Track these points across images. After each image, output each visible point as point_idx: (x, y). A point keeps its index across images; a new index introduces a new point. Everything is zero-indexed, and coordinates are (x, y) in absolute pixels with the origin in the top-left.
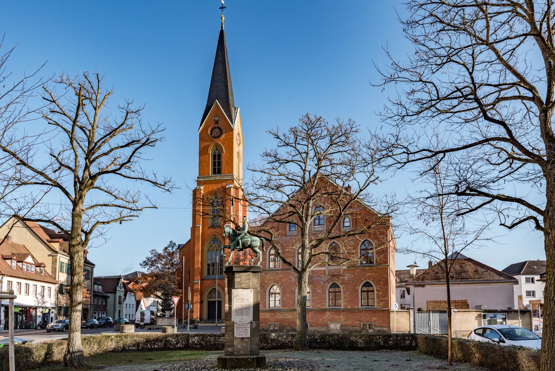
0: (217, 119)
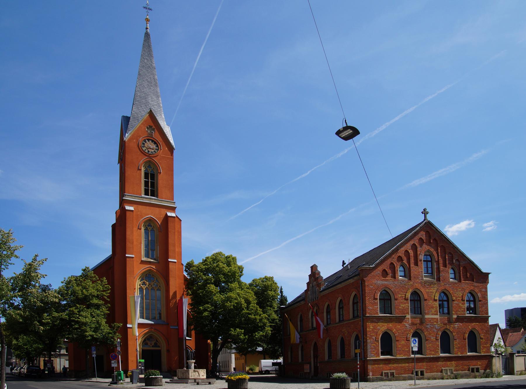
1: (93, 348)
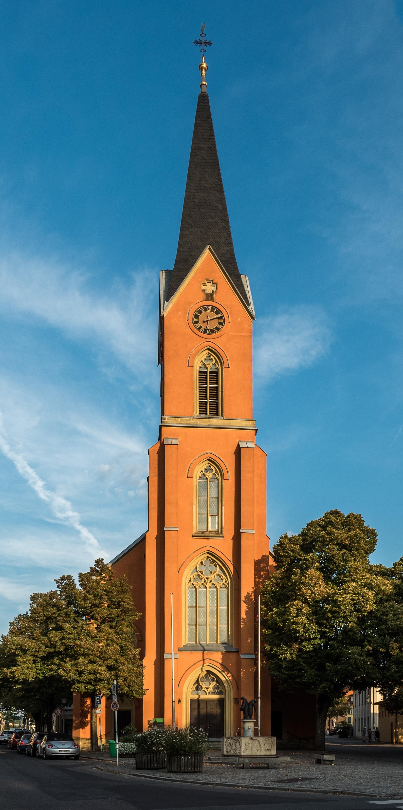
0: (209, 288)
1: (97, 698)
